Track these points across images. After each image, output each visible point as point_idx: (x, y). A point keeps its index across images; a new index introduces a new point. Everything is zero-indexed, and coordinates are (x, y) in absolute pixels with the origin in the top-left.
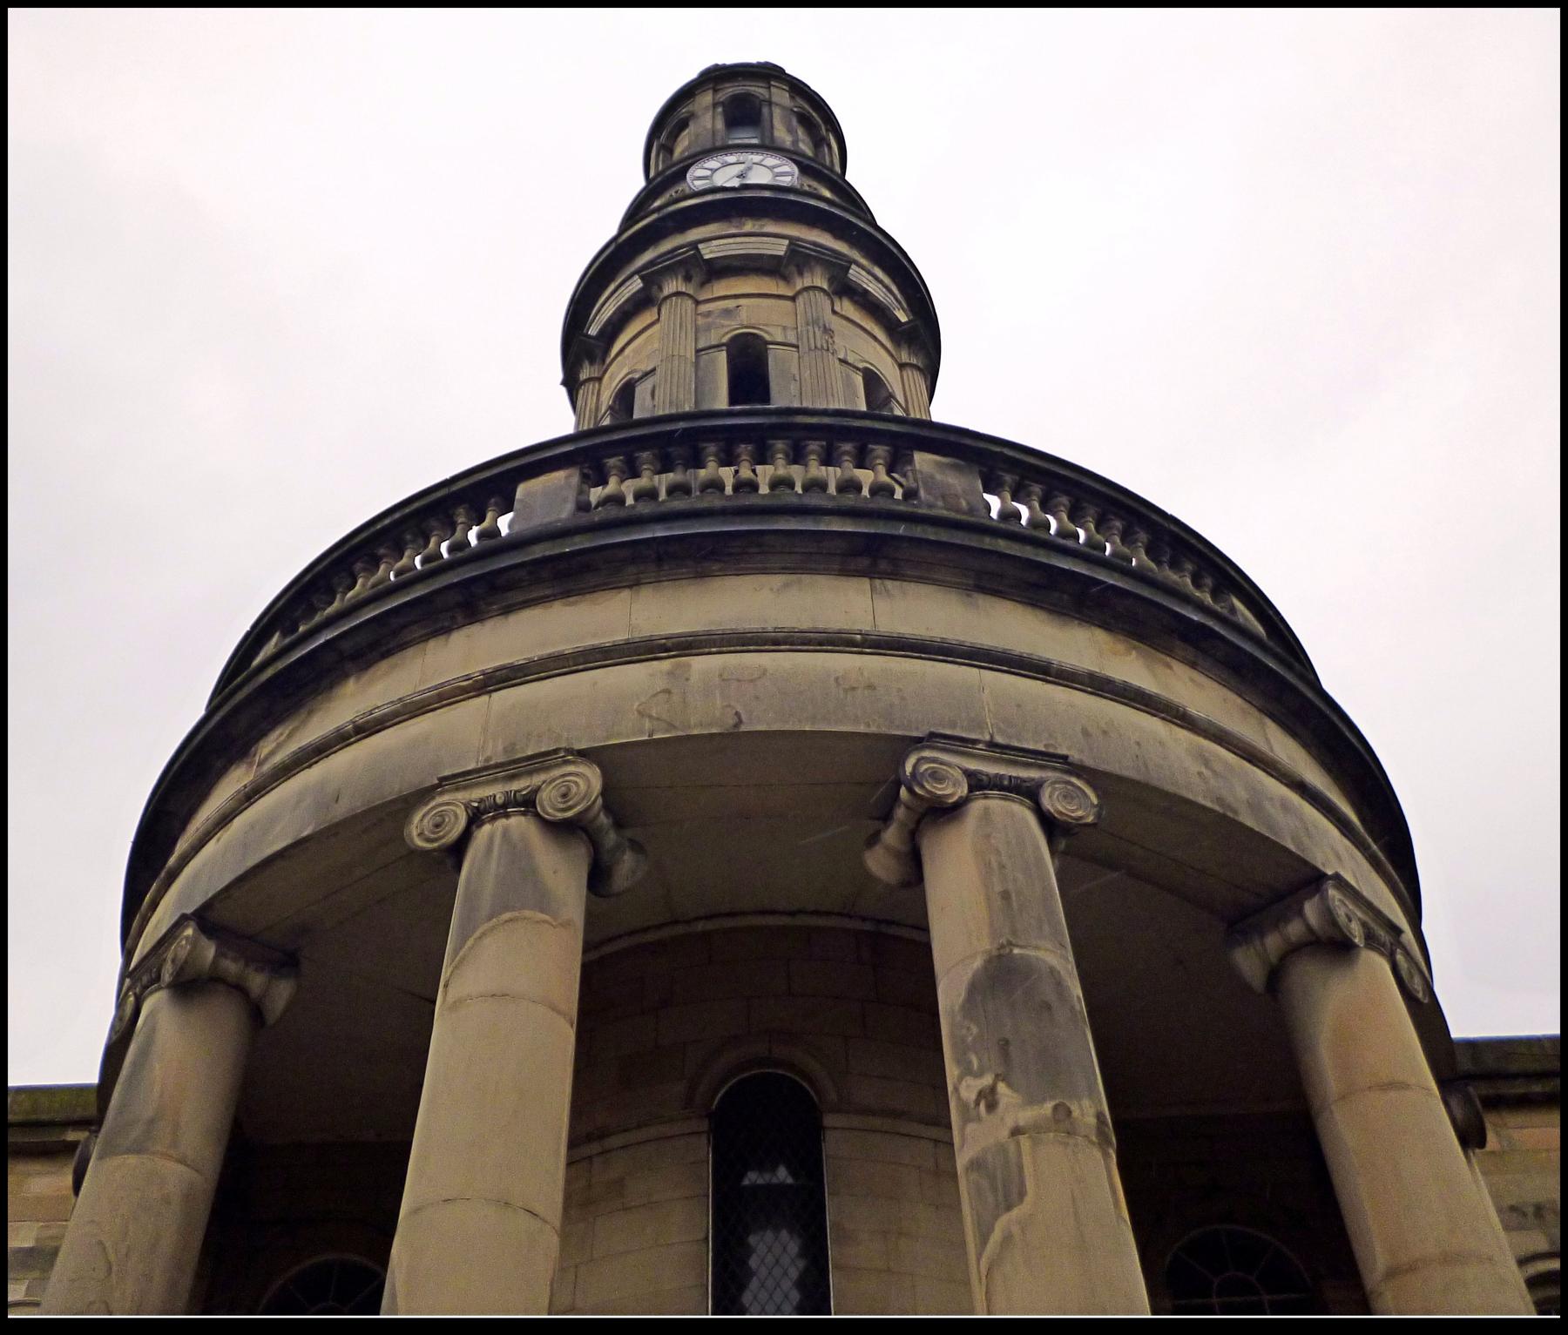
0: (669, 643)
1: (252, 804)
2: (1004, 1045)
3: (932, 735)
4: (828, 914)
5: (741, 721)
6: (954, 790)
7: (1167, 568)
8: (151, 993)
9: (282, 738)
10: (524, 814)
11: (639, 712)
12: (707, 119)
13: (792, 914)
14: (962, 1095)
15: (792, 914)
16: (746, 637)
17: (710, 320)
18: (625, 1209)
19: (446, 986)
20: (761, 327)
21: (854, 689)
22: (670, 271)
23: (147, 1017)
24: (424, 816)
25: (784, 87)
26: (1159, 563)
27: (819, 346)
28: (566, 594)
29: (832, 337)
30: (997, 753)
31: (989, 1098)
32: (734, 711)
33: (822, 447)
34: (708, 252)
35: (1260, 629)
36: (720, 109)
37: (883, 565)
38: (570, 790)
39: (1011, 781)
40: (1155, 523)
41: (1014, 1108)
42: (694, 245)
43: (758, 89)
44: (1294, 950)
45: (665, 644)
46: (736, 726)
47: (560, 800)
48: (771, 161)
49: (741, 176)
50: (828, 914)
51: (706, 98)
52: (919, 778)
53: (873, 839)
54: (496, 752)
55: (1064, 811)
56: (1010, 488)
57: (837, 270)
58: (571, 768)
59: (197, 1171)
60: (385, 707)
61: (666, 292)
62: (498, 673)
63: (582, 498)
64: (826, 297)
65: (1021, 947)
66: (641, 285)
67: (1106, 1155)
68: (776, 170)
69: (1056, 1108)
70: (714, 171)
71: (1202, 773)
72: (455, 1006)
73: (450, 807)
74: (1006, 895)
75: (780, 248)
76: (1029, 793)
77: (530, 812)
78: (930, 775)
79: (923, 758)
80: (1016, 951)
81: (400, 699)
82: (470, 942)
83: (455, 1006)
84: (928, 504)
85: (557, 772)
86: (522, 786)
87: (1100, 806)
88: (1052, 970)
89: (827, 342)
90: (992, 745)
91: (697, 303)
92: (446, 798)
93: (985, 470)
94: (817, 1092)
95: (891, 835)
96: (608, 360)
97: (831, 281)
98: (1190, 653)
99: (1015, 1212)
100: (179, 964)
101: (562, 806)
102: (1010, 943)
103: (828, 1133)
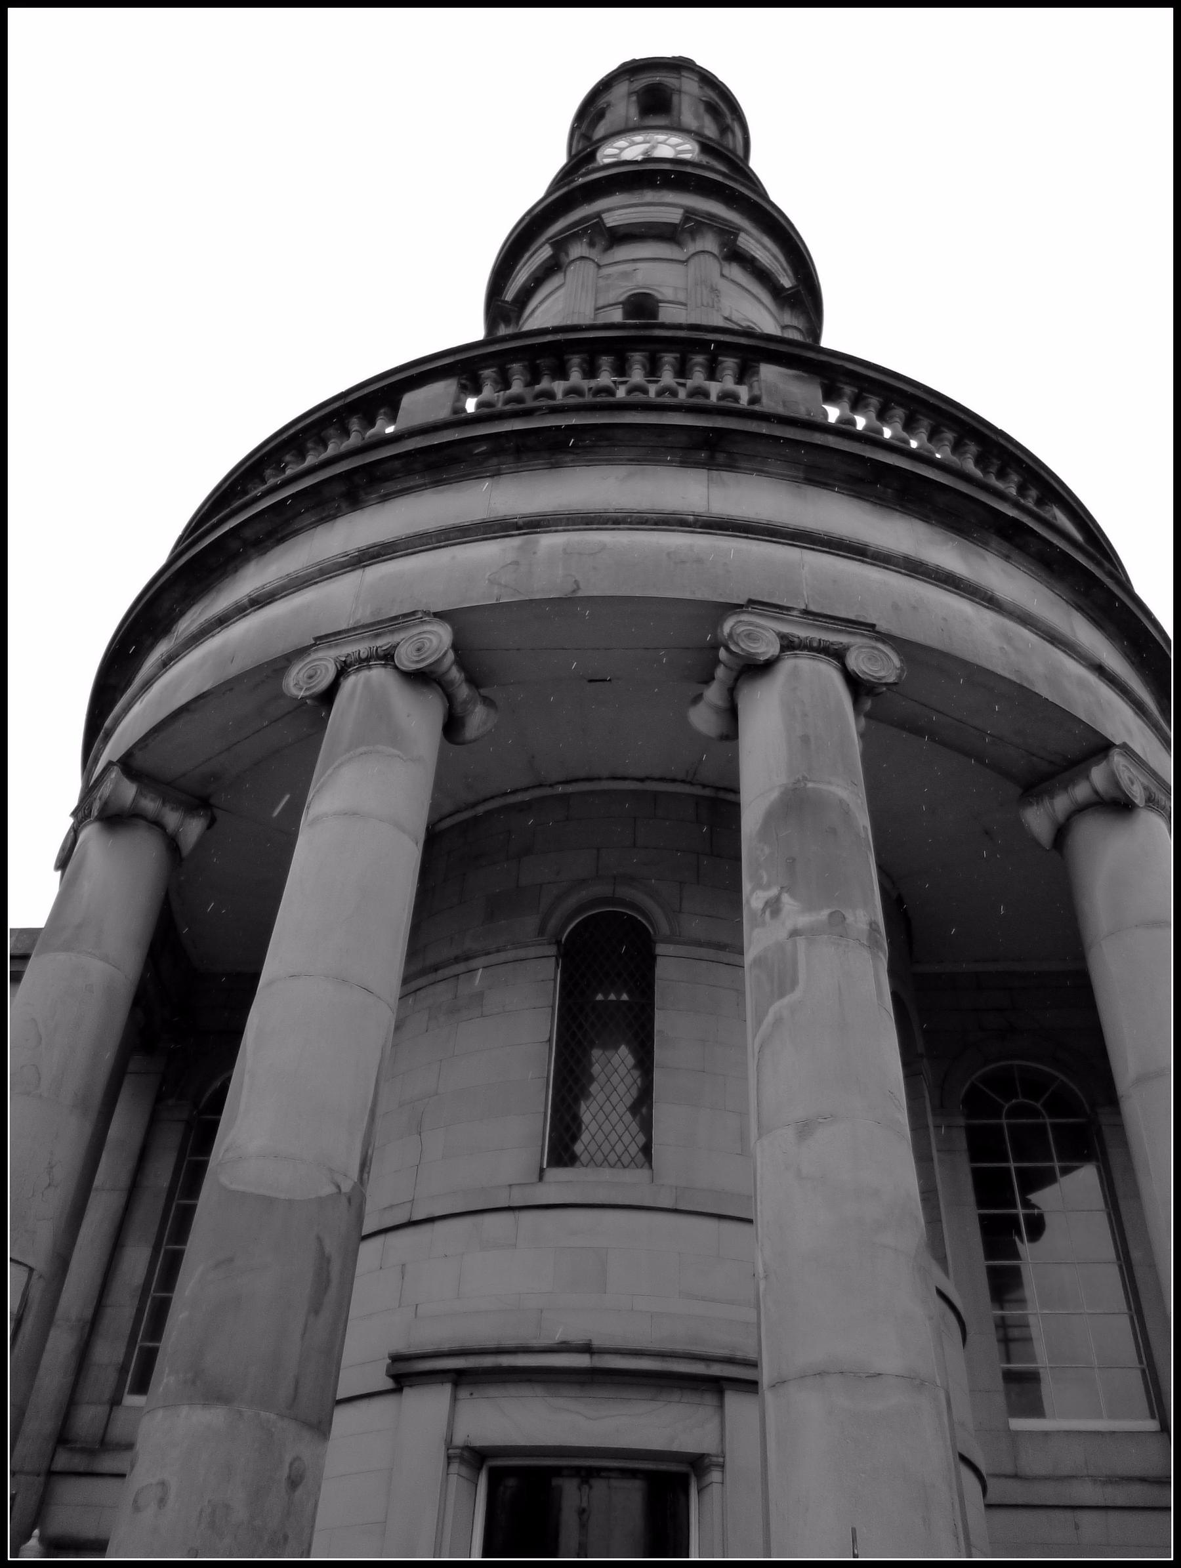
0: (521, 522)
1: (167, 670)
2: (791, 863)
3: (751, 602)
4: (674, 780)
5: (578, 588)
6: (766, 648)
7: (994, 478)
8: (85, 826)
9: (195, 616)
10: (384, 666)
11: (489, 580)
12: (622, 106)
13: (642, 780)
14: (752, 906)
15: (642, 780)
16: (590, 517)
17: (609, 282)
18: (482, 1016)
19: (308, 808)
20: (655, 288)
21: (683, 562)
22: (576, 237)
23: (80, 845)
24: (299, 671)
25: (693, 77)
26: (985, 471)
27: (705, 304)
28: (437, 483)
29: (718, 296)
30: (811, 620)
31: (774, 907)
32: (574, 579)
33: (676, 358)
34: (611, 220)
35: (1079, 537)
36: (634, 98)
37: (721, 458)
38: (424, 645)
39: (820, 642)
40: (985, 436)
41: (794, 914)
42: (598, 215)
43: (669, 80)
44: (1081, 809)
45: (517, 522)
46: (574, 591)
47: (415, 654)
48: (675, 140)
49: (646, 153)
50: (674, 780)
51: (621, 88)
52: (735, 638)
53: (698, 699)
54: (364, 615)
55: (866, 671)
56: (849, 399)
57: (727, 234)
58: (427, 628)
59: (116, 967)
60: (275, 582)
61: (572, 257)
62: (371, 550)
63: (459, 404)
64: (715, 261)
65: (814, 781)
66: (551, 252)
67: (875, 957)
68: (679, 148)
69: (831, 915)
70: (622, 149)
71: (1004, 648)
72: (316, 820)
73: (322, 662)
74: (805, 739)
75: (674, 216)
76: (837, 655)
77: (389, 664)
78: (745, 636)
79: (740, 621)
80: (810, 785)
81: (287, 575)
82: (329, 772)
83: (316, 820)
84: (768, 405)
85: (415, 631)
86: (383, 643)
87: (902, 669)
88: (841, 801)
89: (713, 299)
90: (806, 612)
91: (599, 266)
92: (320, 654)
93: (826, 382)
94: (653, 929)
95: (714, 694)
96: (521, 323)
97: (723, 245)
98: (1005, 547)
99: (786, 1000)
100: (103, 800)
101: (417, 659)
102: (805, 778)
103: (659, 959)
